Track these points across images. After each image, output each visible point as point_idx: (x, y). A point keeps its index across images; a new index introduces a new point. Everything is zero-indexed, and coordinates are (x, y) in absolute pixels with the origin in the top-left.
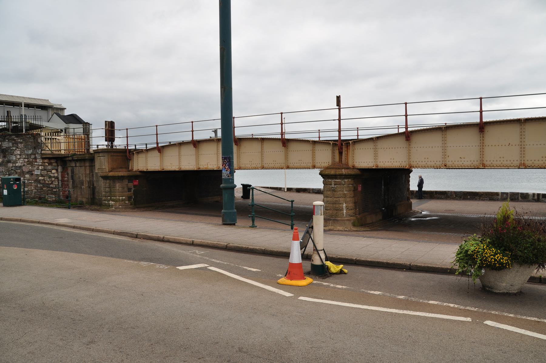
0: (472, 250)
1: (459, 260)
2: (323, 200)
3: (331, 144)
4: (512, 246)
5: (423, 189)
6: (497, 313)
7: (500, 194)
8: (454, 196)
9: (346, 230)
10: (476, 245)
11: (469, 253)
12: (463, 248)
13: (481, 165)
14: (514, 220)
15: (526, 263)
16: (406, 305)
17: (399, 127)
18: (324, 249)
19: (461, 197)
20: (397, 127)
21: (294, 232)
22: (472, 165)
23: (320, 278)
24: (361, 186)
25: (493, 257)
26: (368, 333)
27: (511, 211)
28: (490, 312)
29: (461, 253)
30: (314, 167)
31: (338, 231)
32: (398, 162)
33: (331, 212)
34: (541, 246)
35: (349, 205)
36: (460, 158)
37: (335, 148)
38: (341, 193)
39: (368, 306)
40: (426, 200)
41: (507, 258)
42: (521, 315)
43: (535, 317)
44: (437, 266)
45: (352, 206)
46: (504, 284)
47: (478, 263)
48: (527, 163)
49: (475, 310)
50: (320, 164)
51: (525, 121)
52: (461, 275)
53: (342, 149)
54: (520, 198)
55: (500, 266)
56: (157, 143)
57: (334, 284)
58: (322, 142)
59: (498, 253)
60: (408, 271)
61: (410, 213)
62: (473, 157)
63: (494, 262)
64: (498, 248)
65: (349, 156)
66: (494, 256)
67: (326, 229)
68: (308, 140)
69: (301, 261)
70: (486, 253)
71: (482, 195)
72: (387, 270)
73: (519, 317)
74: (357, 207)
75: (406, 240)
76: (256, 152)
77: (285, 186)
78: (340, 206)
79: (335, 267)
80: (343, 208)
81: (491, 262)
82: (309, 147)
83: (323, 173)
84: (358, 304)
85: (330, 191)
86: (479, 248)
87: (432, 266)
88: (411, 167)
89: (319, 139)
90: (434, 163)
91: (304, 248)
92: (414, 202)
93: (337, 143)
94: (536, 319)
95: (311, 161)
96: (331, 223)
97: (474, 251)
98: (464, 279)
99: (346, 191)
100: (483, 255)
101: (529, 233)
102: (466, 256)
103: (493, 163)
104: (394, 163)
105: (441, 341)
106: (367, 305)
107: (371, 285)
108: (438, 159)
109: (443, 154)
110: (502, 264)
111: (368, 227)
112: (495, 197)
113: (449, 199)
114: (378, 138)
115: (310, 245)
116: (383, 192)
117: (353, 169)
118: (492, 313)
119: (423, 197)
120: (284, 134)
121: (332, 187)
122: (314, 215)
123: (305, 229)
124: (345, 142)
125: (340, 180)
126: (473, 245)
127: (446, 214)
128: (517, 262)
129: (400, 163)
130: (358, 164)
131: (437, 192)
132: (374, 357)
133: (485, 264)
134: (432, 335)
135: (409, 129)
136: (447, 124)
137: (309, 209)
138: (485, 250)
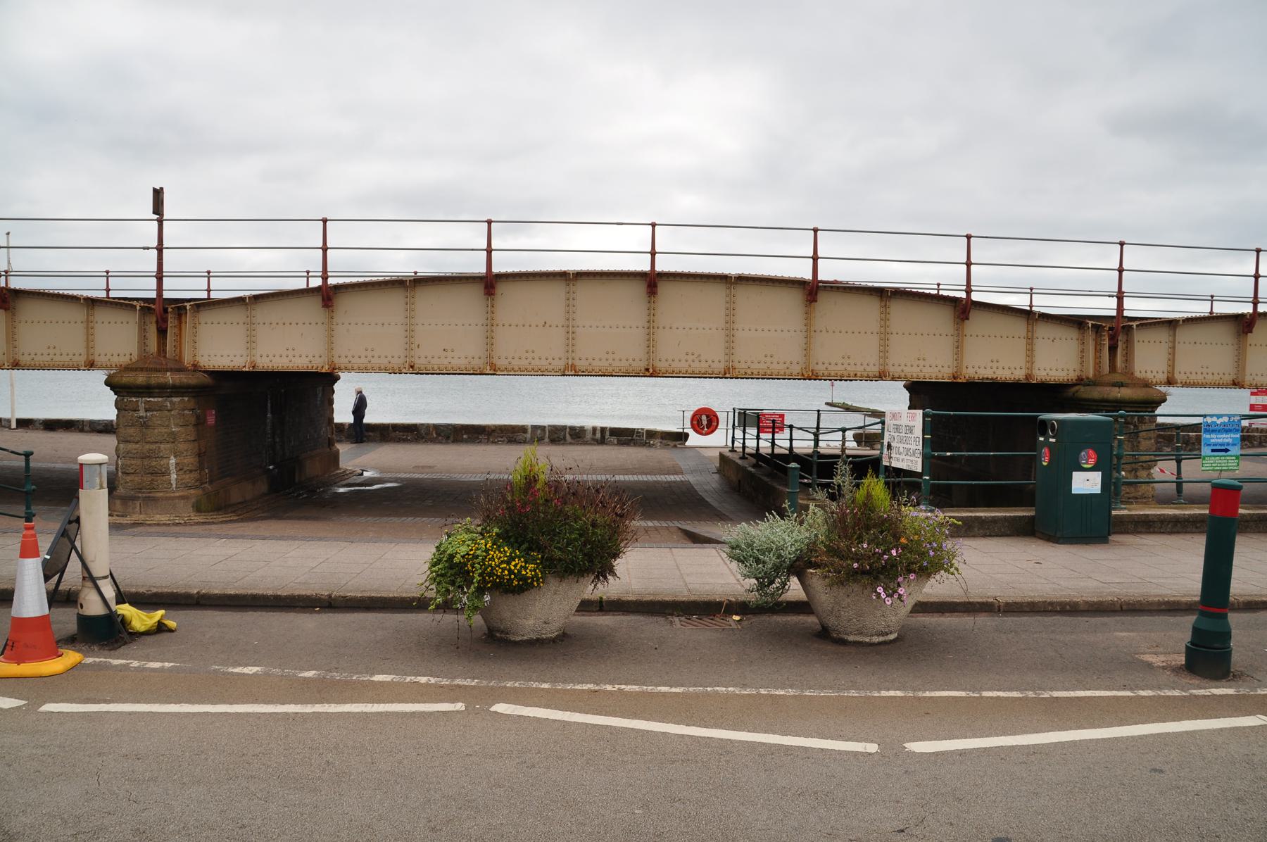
0: (462, 554)
1: (438, 578)
2: (116, 450)
3: (138, 308)
4: (544, 540)
5: (366, 420)
6: (517, 684)
7: (530, 430)
8: (435, 435)
9: (177, 521)
10: (470, 542)
11: (456, 560)
12: (444, 552)
13: (488, 368)
14: (546, 484)
15: (571, 574)
16: (319, 692)
17: (310, 274)
18: (111, 574)
19: (448, 438)
20: (305, 274)
21: (24, 536)
22: (769, 372)
23: (104, 650)
24: (214, 413)
25: (505, 565)
26: (227, 770)
27: (541, 465)
28: (503, 684)
29: (439, 561)
30: (91, 365)
31: (158, 525)
33: (137, 479)
34: (598, 537)
35: (186, 461)
36: (444, 350)
37: (147, 320)
38: (164, 430)
39: (228, 705)
40: (372, 445)
41: (533, 565)
42: (565, 682)
43: (590, 683)
44: (391, 595)
45: (192, 464)
46: (531, 622)
47: (475, 581)
48: (581, 364)
49: (473, 684)
51: (576, 277)
52: (443, 611)
53: (165, 321)
54: (568, 437)
55: (521, 583)
57: (139, 660)
58: (111, 303)
59: (516, 556)
60: (326, 612)
61: (334, 475)
62: (469, 349)
63: (508, 577)
64: (516, 545)
65: (183, 341)
66: (508, 563)
67: (126, 522)
68: (75, 294)
69: (47, 611)
70: (492, 559)
71: (493, 431)
72: (275, 613)
73: (560, 686)
74: (206, 466)
75: (320, 539)
77: (13, 412)
78: (162, 463)
79: (145, 618)
80: (169, 469)
81: (501, 577)
82: (77, 314)
83: (116, 380)
84: (203, 703)
85: (133, 425)
86: (477, 549)
87: (379, 595)
88: (334, 369)
89: (108, 294)
90: (386, 361)
91: (58, 575)
92: (343, 449)
93: (153, 307)
94: (592, 686)
95: (83, 351)
96: (138, 508)
97: (467, 556)
98: (449, 618)
99: (177, 425)
100: (486, 563)
101: (576, 510)
102: (451, 568)
103: (514, 362)
104: (293, 359)
105: (400, 762)
106: (224, 702)
107: (236, 654)
108: (394, 351)
109: (887, 348)
110: (524, 578)
111: (234, 512)
112: (520, 436)
113: (424, 440)
114: (258, 299)
115: (74, 566)
116: (269, 428)
117: (194, 371)
118: (508, 685)
119: (365, 439)
121: (140, 417)
122: (82, 489)
123: (56, 526)
124: (173, 306)
125: (160, 399)
126: (464, 541)
127: (416, 476)
128: (555, 572)
129: (308, 359)
130: (207, 360)
131: (395, 427)
132: (244, 826)
133: (490, 581)
134: (380, 752)
135: (331, 281)
136: (418, 274)
137: (69, 471)
138: (490, 552)
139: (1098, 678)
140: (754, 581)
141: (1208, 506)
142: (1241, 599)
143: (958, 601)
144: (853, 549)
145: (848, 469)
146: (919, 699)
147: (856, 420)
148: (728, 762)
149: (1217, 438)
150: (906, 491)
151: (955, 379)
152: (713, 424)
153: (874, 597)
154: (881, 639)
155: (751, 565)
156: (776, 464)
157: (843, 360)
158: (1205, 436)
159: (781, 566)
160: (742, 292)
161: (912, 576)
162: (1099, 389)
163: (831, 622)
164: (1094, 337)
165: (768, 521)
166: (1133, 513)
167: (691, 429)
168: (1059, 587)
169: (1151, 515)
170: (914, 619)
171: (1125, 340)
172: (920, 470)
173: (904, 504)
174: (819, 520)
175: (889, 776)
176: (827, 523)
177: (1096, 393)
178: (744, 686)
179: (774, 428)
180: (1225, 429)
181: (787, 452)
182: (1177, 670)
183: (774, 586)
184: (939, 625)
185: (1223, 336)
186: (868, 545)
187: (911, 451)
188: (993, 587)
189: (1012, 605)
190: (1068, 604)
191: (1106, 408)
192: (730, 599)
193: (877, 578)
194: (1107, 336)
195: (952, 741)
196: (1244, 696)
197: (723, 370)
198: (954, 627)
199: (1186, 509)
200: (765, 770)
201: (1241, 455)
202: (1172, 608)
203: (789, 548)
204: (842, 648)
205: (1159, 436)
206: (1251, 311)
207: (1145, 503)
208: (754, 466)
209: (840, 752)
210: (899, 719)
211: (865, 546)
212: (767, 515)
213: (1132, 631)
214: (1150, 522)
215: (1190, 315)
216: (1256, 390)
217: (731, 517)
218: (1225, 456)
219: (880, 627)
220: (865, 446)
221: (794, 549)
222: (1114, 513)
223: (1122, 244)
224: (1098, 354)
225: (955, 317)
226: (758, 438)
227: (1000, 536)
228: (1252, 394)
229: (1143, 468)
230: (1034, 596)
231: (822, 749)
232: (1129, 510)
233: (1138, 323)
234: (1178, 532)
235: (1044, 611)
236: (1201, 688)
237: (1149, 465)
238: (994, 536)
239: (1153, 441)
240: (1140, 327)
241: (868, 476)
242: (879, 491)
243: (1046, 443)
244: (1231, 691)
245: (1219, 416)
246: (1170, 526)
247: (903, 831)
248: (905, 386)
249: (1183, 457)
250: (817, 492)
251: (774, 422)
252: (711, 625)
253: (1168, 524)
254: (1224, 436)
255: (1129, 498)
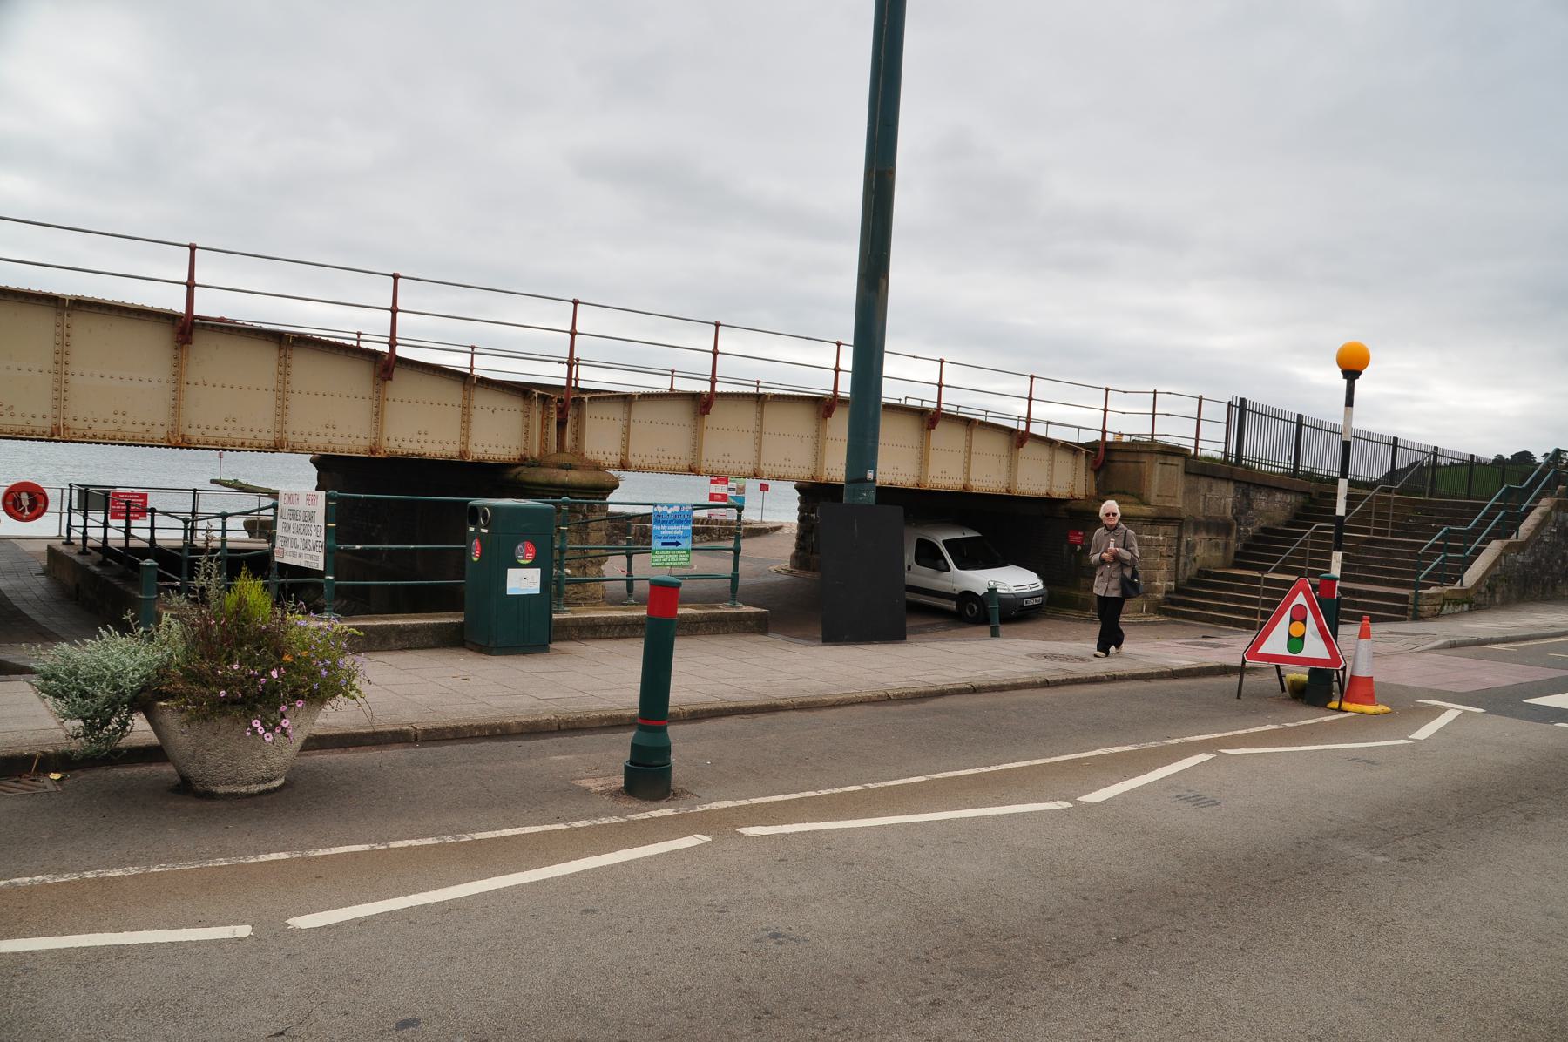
22: (119, 435)
32: (247, 430)
50: (200, 431)
56: (1104, 432)
76: (679, 425)
109: (285, 411)
120: (577, 365)
139: (529, 812)
140: (79, 723)
141: (646, 606)
142: (686, 709)
143: (364, 731)
144: (219, 672)
145: (215, 567)
146: (309, 859)
147: (249, 502)
148: (24, 985)
149: (667, 530)
150: (293, 595)
151: (372, 453)
152: (39, 505)
153: (249, 734)
154: (262, 787)
155: (73, 701)
156: (125, 559)
157: (115, 417)
158: (655, 527)
159: (119, 699)
160: (82, 326)
161: (300, 704)
162: (545, 471)
163: (193, 770)
164: (541, 409)
165: (101, 638)
166: (578, 616)
167: (4, 513)
168: (489, 707)
169: (598, 618)
170: (308, 758)
171: (575, 415)
172: (321, 568)
173: (290, 612)
174: (176, 637)
175: (265, 964)
176: (186, 639)
177: (541, 476)
178: (61, 871)
179: (128, 511)
180: (676, 520)
181: (147, 545)
182: (615, 794)
183: (110, 727)
184: (340, 763)
185: (680, 414)
186: (241, 665)
187: (311, 544)
188: (409, 711)
189: (431, 732)
190: (499, 726)
191: (552, 494)
192: (46, 750)
193: (253, 709)
194: (555, 409)
195: (349, 908)
196: (683, 814)
197: (49, 431)
198: (360, 765)
199: (635, 610)
200: (86, 986)
201: (692, 549)
202: (613, 724)
203: (131, 675)
204: (209, 803)
205: (615, 527)
206: (709, 390)
207: (595, 605)
208: (99, 564)
209: (198, 943)
210: (282, 888)
211: (236, 667)
212: (101, 630)
213: (570, 753)
214: (596, 626)
215: (646, 390)
216: (716, 478)
217: (63, 636)
218: (676, 550)
219: (261, 770)
220: (260, 537)
221: (137, 676)
222: (555, 616)
223: (576, 303)
224: (545, 430)
225: (374, 376)
226: (106, 525)
227: (422, 648)
228: (712, 482)
229: (593, 564)
230: (459, 720)
231: (173, 943)
232: (573, 612)
233: (590, 396)
234: (626, 637)
235: (470, 737)
236: (640, 812)
237: (599, 561)
238: (415, 649)
239: (604, 533)
240: (642, 398)
241: (242, 577)
242: (256, 596)
243: (478, 534)
244: (670, 812)
245: (670, 505)
246: (618, 630)
247: (282, 1034)
248: (312, 461)
249: (635, 551)
250: (171, 598)
251: (128, 504)
252: (15, 790)
253: (616, 628)
254: (675, 528)
255: (577, 599)
